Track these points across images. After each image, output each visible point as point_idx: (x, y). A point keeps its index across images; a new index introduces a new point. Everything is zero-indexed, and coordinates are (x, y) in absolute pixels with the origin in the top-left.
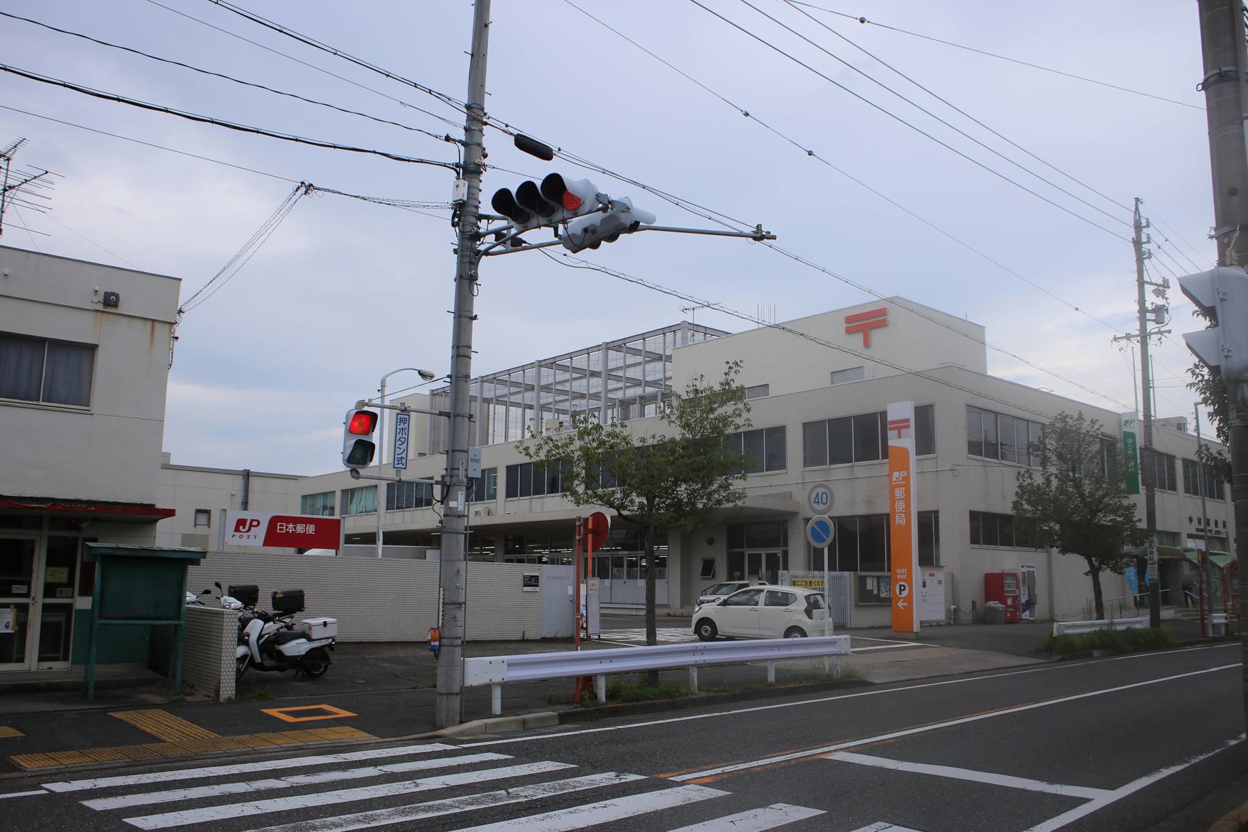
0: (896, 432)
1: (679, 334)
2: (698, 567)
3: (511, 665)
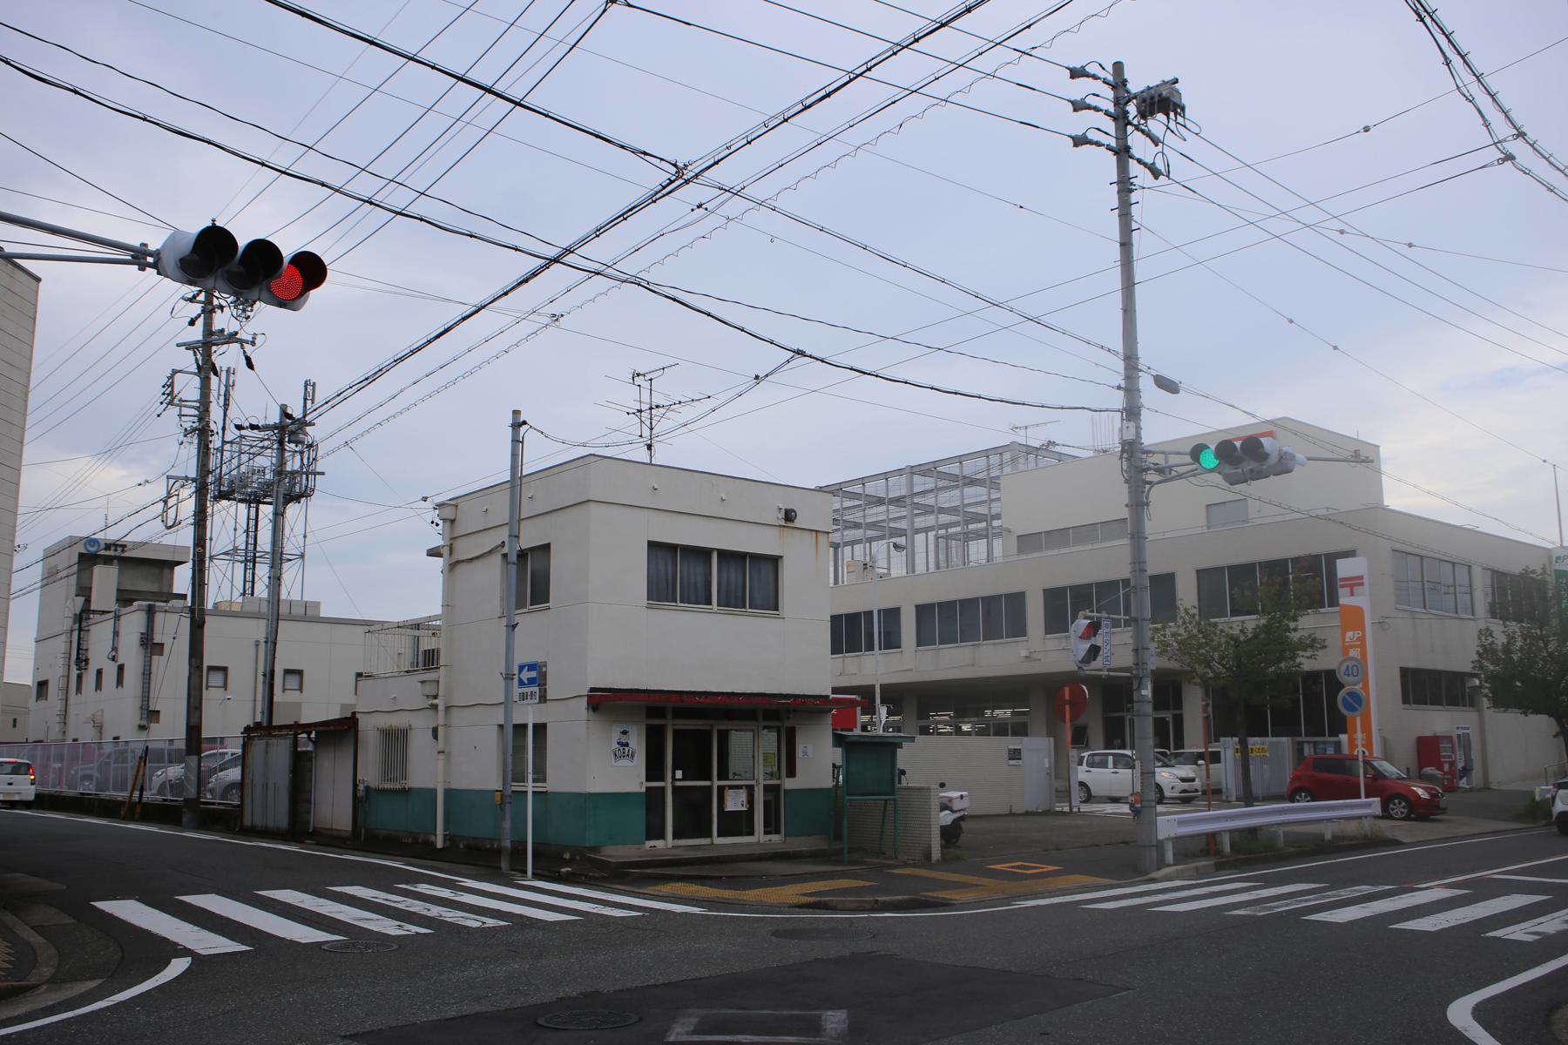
1: (1007, 456)
3: (1181, 823)
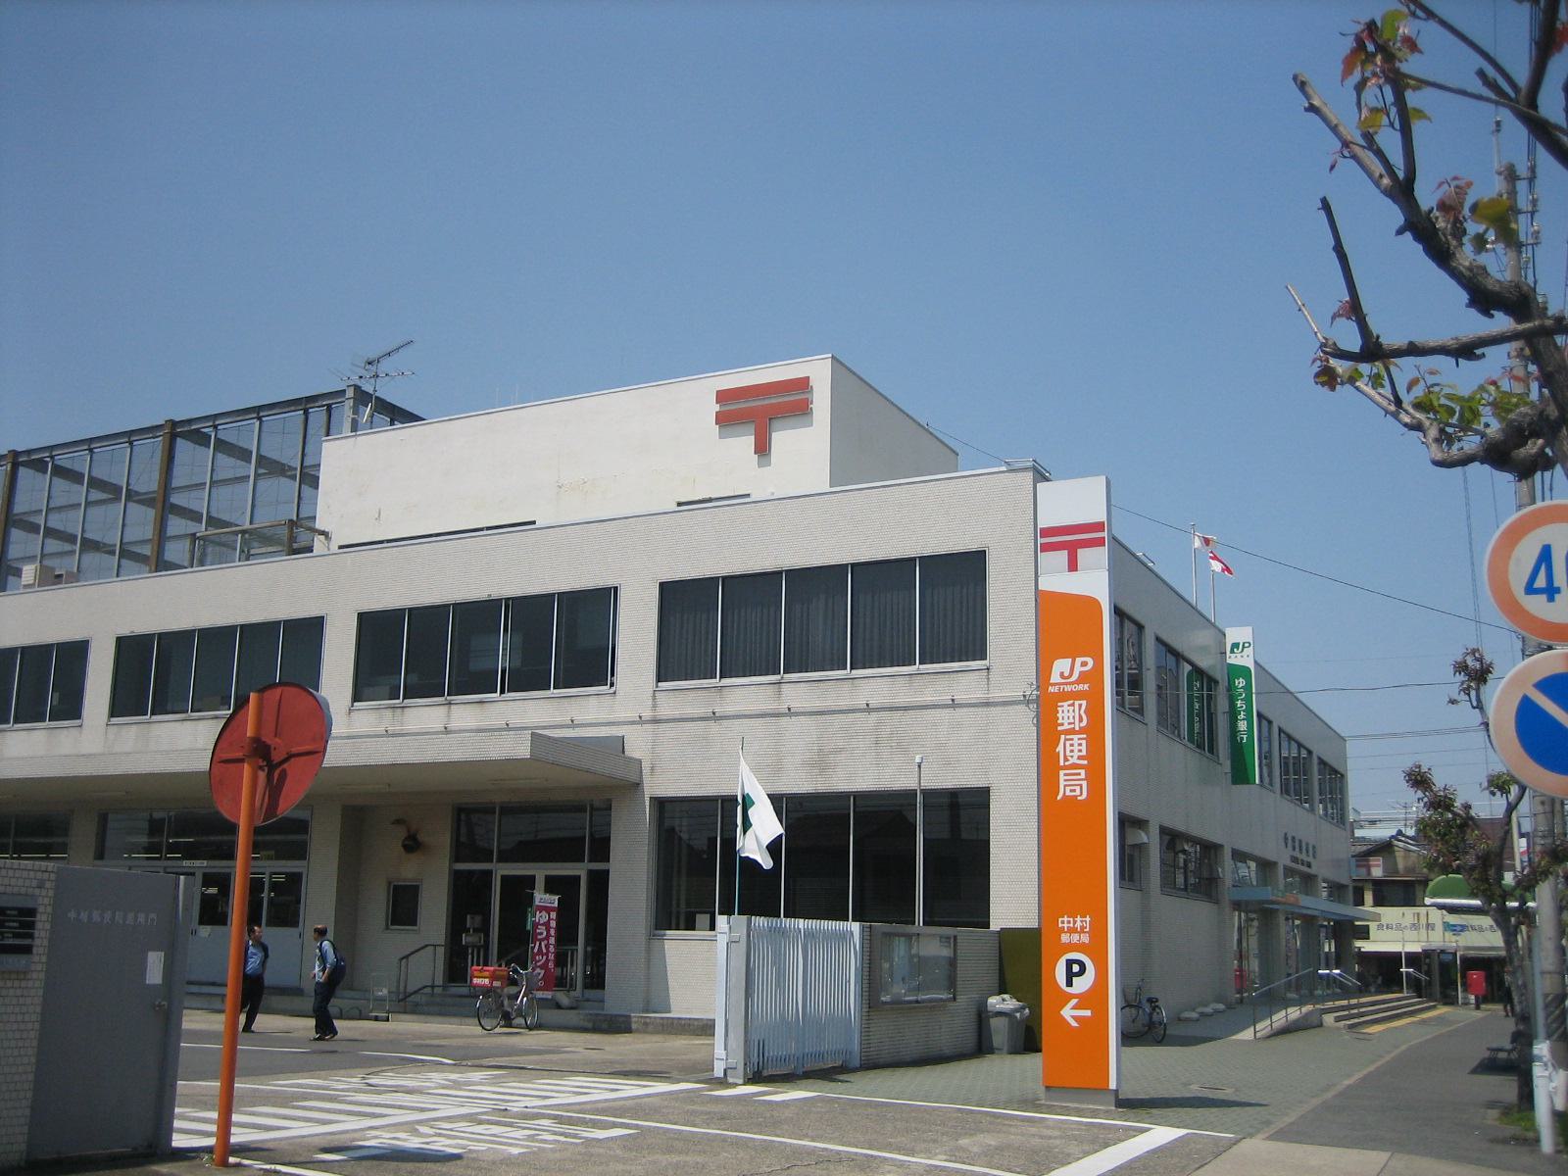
0: (1063, 556)
2: (377, 905)
